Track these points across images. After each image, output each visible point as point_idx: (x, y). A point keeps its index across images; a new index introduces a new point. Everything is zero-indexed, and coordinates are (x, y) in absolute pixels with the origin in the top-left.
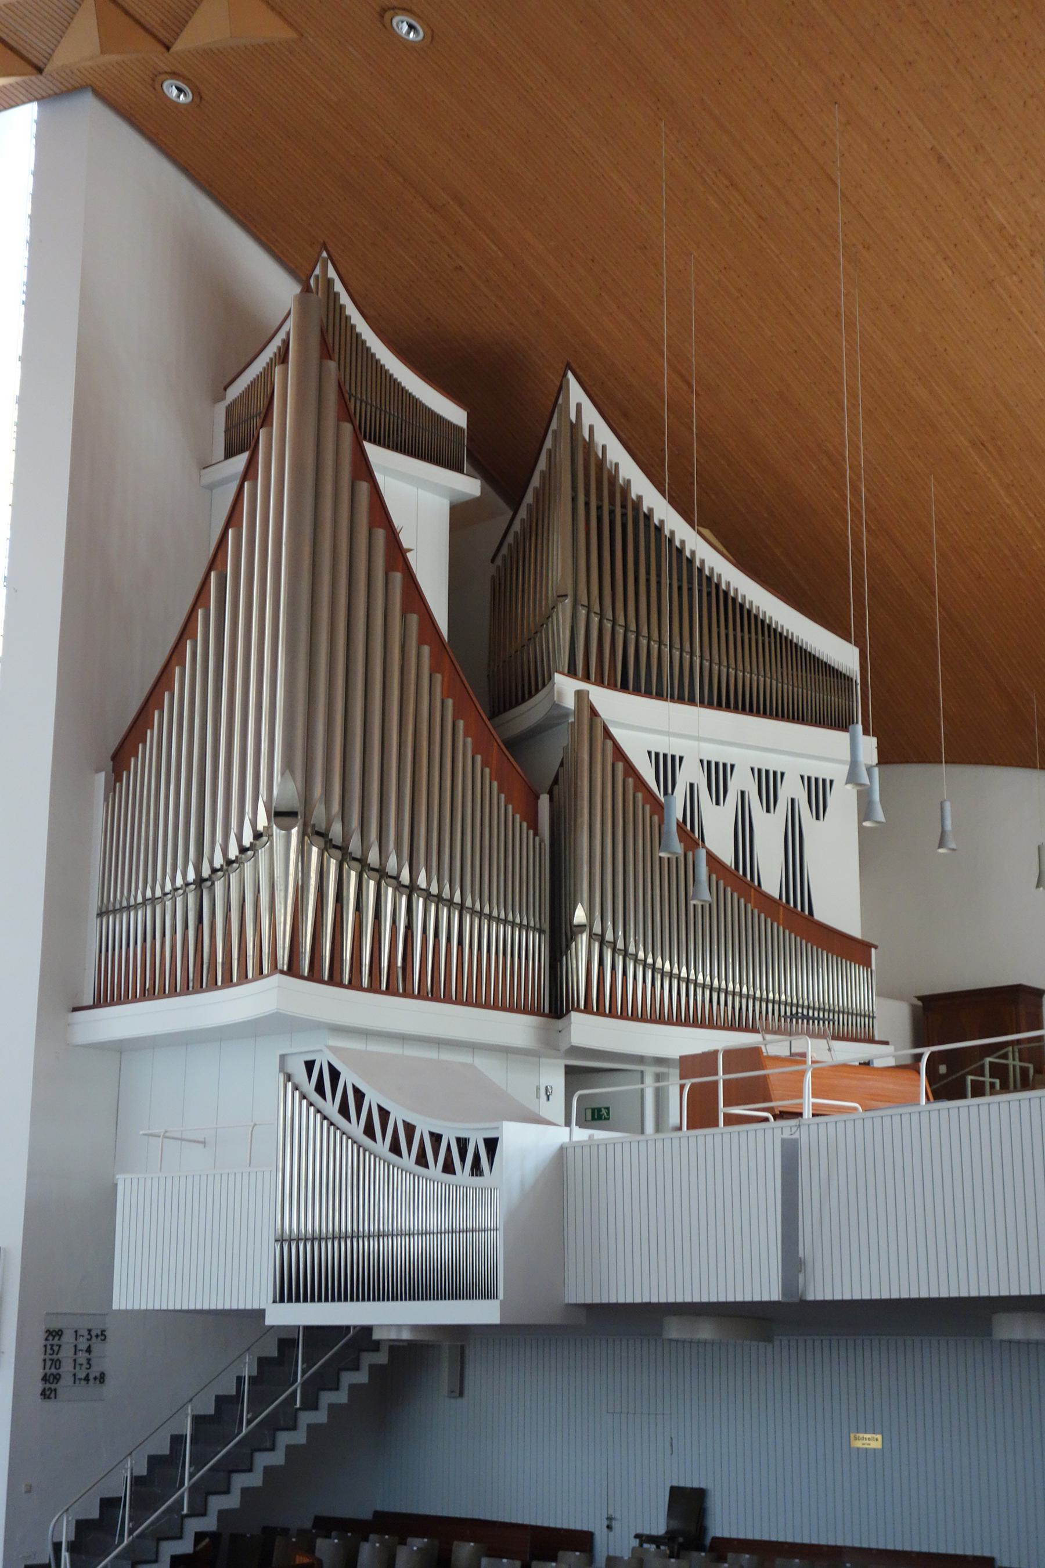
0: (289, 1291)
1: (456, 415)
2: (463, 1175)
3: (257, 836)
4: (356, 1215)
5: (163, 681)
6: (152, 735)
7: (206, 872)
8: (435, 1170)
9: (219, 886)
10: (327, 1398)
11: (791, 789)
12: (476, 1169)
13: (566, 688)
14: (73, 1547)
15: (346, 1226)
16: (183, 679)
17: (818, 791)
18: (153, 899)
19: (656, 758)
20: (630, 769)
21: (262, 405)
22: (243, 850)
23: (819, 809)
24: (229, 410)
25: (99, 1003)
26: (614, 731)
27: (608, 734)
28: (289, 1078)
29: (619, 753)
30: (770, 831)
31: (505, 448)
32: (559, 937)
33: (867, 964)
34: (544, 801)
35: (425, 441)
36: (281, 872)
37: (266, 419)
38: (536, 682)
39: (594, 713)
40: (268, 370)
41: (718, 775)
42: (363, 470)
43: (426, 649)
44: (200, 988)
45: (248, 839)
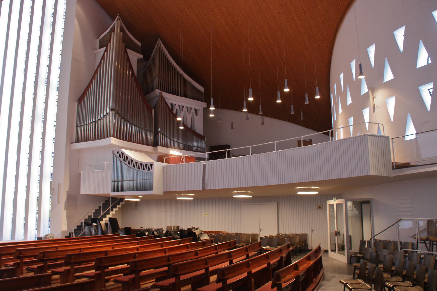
0: (114, 190)
1: (139, 44)
2: (146, 170)
3: (107, 113)
4: (127, 177)
5: (89, 86)
6: (86, 96)
7: (97, 119)
8: (141, 170)
9: (99, 122)
10: (114, 209)
11: (193, 111)
12: (149, 170)
13: (157, 92)
14: (74, 233)
15: (125, 179)
16: (93, 87)
17: (197, 111)
18: (87, 124)
19: (171, 104)
20: (168, 106)
21: (109, 39)
22: (104, 116)
23: (197, 115)
24: (100, 40)
25: (77, 142)
26: (166, 100)
27: (164, 100)
28: (114, 154)
29: (166, 103)
30: (189, 117)
31: (146, 51)
32: (156, 134)
33: (204, 140)
34: (153, 110)
35: (135, 48)
36: (111, 120)
37: (110, 41)
38: (152, 90)
39: (162, 96)
40: (110, 33)
41: (181, 107)
42: (126, 52)
43: (135, 83)
44: (95, 140)
45: (105, 114)
